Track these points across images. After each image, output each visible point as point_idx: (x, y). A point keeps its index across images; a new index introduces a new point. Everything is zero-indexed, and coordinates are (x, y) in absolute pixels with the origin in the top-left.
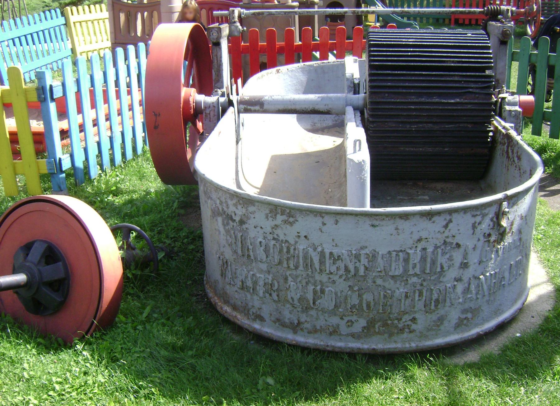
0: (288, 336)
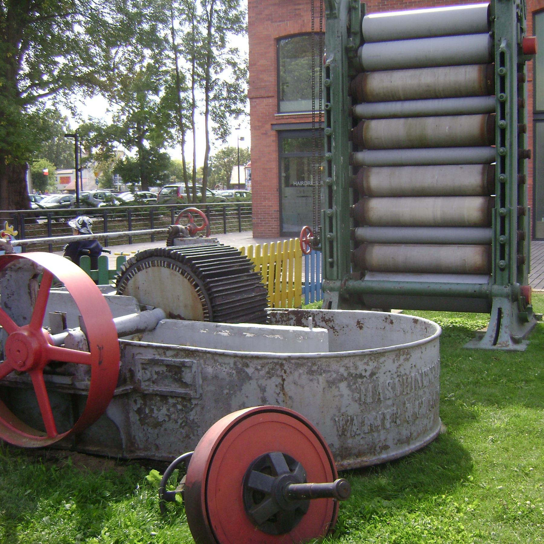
0: (407, 449)
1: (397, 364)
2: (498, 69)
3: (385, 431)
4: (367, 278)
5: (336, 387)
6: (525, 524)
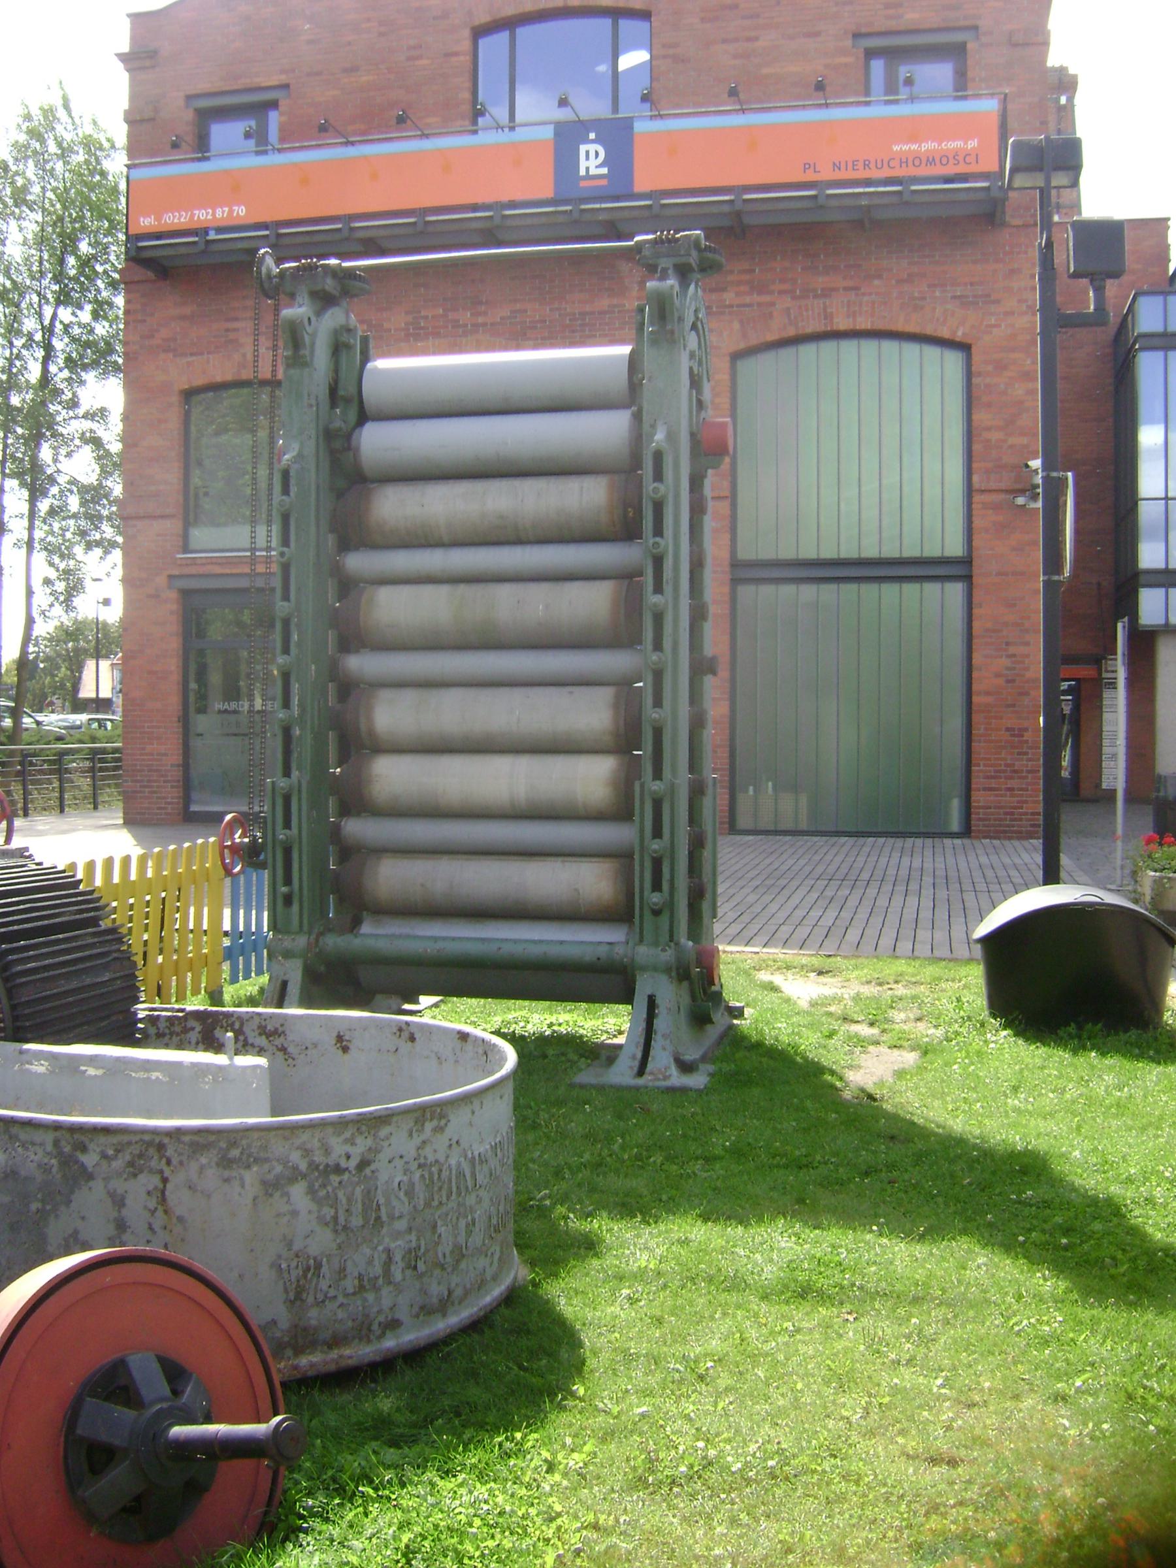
0: (441, 1326)
1: (417, 1140)
2: (649, 486)
3: (391, 1288)
4: (366, 928)
5: (282, 1196)
6: (693, 1496)
